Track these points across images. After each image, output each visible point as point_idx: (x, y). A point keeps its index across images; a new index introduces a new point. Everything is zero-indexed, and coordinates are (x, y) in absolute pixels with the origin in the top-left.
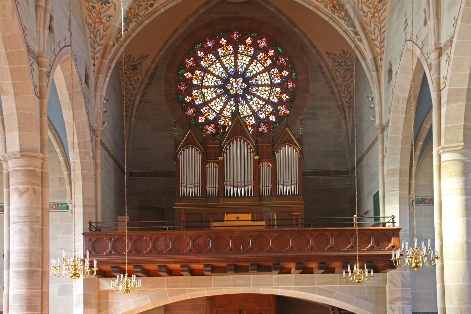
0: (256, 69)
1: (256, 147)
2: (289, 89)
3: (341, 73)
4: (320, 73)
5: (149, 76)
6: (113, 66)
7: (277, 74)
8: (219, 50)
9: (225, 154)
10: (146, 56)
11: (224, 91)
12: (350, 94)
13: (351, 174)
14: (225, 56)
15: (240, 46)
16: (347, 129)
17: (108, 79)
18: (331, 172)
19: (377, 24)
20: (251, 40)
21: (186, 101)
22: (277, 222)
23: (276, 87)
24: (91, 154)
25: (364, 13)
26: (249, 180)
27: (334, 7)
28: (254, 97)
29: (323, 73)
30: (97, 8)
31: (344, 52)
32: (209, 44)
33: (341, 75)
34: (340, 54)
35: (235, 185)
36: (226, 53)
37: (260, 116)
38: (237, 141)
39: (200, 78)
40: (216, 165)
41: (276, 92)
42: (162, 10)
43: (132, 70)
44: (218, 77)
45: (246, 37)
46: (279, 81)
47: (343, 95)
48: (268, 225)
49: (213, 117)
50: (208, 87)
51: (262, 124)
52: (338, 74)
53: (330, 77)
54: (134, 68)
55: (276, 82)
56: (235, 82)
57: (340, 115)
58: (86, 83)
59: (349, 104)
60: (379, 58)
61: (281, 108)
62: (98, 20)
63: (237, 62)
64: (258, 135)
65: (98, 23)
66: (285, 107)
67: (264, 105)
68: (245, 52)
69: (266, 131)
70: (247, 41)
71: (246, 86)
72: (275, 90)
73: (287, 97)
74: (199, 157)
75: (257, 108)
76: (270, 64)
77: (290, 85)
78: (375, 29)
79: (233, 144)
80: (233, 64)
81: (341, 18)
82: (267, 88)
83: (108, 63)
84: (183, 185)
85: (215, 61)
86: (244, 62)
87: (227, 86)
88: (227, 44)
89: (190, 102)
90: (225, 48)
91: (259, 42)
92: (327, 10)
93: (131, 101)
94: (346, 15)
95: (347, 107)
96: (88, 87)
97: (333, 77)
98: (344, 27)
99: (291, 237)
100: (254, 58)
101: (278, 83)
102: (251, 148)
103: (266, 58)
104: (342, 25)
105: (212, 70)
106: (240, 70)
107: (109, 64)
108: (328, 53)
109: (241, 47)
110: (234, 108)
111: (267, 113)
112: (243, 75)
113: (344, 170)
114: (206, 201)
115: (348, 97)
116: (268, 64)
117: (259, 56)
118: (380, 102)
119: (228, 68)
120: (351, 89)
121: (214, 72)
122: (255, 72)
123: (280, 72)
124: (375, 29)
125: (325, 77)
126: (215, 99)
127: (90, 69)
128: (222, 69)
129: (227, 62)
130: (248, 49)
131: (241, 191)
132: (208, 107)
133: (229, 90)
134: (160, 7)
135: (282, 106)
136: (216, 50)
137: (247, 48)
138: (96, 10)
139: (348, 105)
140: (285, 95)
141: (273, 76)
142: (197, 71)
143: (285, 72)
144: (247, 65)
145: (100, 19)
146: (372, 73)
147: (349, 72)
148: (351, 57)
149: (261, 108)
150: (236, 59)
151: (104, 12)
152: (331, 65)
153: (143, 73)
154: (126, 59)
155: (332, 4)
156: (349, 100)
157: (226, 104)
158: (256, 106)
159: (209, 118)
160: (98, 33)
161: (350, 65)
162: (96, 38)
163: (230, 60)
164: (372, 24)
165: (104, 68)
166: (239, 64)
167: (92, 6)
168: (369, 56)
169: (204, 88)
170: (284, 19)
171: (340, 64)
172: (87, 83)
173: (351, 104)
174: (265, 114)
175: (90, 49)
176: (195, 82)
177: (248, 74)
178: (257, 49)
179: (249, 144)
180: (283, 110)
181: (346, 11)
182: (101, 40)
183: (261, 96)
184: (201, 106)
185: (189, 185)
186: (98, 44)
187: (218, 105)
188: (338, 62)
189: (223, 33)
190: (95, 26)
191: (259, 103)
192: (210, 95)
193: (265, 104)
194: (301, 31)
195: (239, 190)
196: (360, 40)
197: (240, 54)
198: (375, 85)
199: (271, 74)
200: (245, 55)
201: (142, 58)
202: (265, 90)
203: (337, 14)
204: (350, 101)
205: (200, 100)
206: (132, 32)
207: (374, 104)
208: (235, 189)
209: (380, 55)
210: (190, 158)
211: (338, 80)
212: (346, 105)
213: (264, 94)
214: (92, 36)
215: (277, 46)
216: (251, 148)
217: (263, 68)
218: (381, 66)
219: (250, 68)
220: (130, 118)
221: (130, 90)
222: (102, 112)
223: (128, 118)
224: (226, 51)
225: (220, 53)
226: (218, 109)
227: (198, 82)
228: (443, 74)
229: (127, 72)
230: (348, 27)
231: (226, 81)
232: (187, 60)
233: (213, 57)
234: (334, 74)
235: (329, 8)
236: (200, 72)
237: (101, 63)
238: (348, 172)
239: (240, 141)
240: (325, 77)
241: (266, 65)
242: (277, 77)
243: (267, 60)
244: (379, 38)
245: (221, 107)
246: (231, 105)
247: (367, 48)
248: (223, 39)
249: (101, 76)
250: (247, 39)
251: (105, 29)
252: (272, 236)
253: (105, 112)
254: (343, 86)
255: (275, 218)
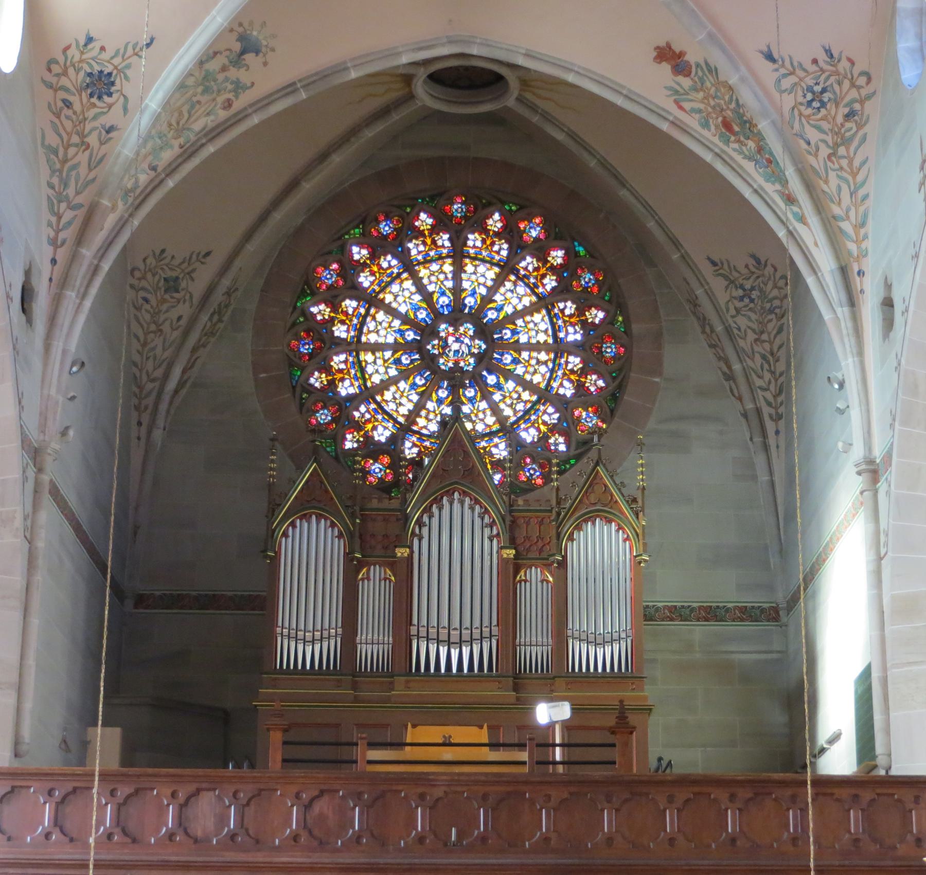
0: (515, 301)
1: (508, 519)
2: (606, 362)
3: (750, 319)
4: (693, 318)
5: (212, 310)
6: (106, 266)
7: (571, 316)
8: (410, 245)
9: (416, 541)
10: (208, 254)
11: (422, 358)
12: (776, 380)
13: (784, 619)
14: (427, 262)
15: (470, 236)
16: (772, 484)
17: (88, 303)
18: (727, 610)
19: (845, 174)
20: (501, 220)
21: (312, 386)
22: (563, 754)
23: (569, 354)
24: (18, 522)
25: (809, 143)
26: (486, 622)
27: (727, 125)
28: (506, 380)
29: (703, 321)
30: (77, 107)
31: (758, 261)
32: (385, 228)
33: (750, 324)
34: (747, 266)
35: (443, 637)
36: (432, 253)
37: (523, 435)
38: (451, 503)
39: (355, 321)
40: (389, 572)
41: (570, 367)
42: (255, 120)
43: (166, 291)
44: (405, 319)
45: (486, 212)
46: (578, 337)
47: (759, 382)
48: (538, 763)
49: (387, 433)
50: (375, 348)
51: (528, 460)
52: (742, 322)
53: (719, 328)
54: (172, 285)
55: (571, 338)
56: (453, 335)
57: (751, 439)
58: (24, 310)
59: (776, 408)
60: (856, 270)
61: (584, 414)
62: (75, 139)
63: (461, 280)
64: (515, 489)
65: (76, 145)
66: (595, 412)
67: (535, 404)
68: (484, 253)
69: (539, 481)
70: (490, 222)
71: (484, 347)
72: (567, 363)
73: (601, 383)
74: (338, 548)
75: (515, 412)
76: (553, 289)
77: (610, 350)
78: (839, 188)
79: (440, 509)
80: (449, 284)
81: (745, 157)
82: (543, 356)
83: (94, 257)
84: (285, 631)
85: (399, 275)
86: (482, 280)
87: (429, 347)
88: (434, 230)
89: (323, 389)
90: (429, 241)
91: (522, 226)
92: (711, 136)
93: (153, 380)
94: (760, 150)
95: (771, 416)
96: (29, 321)
97: (728, 330)
98: (755, 181)
99: (608, 802)
100: (507, 269)
101: (575, 344)
102: (491, 525)
103: (543, 271)
104: (749, 174)
105: (389, 298)
106: (470, 301)
107: (96, 262)
108: (714, 264)
109: (474, 240)
110: (448, 410)
111: (543, 428)
112: (476, 317)
113: (766, 605)
114: (355, 686)
115: (772, 387)
116: (548, 288)
117: (523, 264)
118: (862, 395)
119: (435, 296)
120: (781, 367)
121: (394, 305)
122: (509, 310)
123: (580, 311)
124: (839, 188)
125: (708, 329)
126: (394, 381)
127: (40, 272)
128: (417, 298)
129: (433, 279)
130: (493, 244)
131: (458, 657)
132: (373, 406)
133: (434, 358)
134: (250, 111)
135: (586, 410)
136: (401, 244)
137: (488, 242)
138: (75, 113)
139: (773, 411)
140: (594, 377)
141: (560, 322)
142: (348, 302)
143: (594, 311)
144: (489, 289)
145: (82, 136)
146: (839, 310)
147: (773, 316)
148: (778, 275)
149: (527, 412)
150: (459, 270)
151: (95, 118)
152: (722, 297)
153: (196, 301)
154: (151, 261)
155: (720, 119)
156: (775, 397)
157: (425, 396)
158: (511, 406)
159: (376, 438)
160: (74, 173)
161: (775, 298)
162: (66, 185)
163: (442, 272)
164: (832, 175)
165: (81, 272)
166: (466, 285)
167: (64, 101)
168: (826, 261)
169: (366, 350)
170: (593, 163)
171: (747, 294)
172: (25, 308)
173: (781, 410)
174: (538, 429)
175: (47, 216)
176: (340, 331)
177: (492, 315)
178: (518, 247)
179: (487, 512)
180: (588, 419)
181: (759, 138)
182: (78, 193)
183: (528, 377)
184: (353, 400)
185: (304, 633)
186: (69, 202)
187: (404, 401)
188: (742, 287)
189: (423, 200)
190: (66, 154)
191: (519, 397)
192: (382, 370)
193: (538, 402)
194: (636, 198)
195: (455, 654)
196: (802, 219)
197: (469, 257)
198: (847, 346)
199: (556, 315)
200: (483, 261)
201: (194, 256)
202: (539, 362)
203: (736, 146)
204: (779, 399)
205: (352, 385)
206: (167, 175)
207: (846, 400)
208: (443, 651)
209: (858, 259)
210: (311, 552)
211: (744, 339)
212: (766, 411)
213: (535, 372)
214: (55, 181)
215: (574, 240)
216: (491, 525)
217: (534, 299)
218: (862, 291)
219: (498, 297)
220: (149, 432)
221: (154, 349)
222: (61, 399)
223: (144, 429)
224: (430, 250)
225: (414, 252)
226: (404, 410)
227: (348, 331)
228: (883, 525)
229: (149, 296)
230: (767, 181)
231: (428, 331)
232: (320, 269)
233: (394, 262)
234: (730, 321)
235: (713, 128)
236: (354, 304)
237: (74, 257)
238: (777, 612)
239: (462, 503)
240: (708, 329)
241: (541, 290)
242: (573, 325)
243: (544, 276)
244: (852, 214)
245: (411, 406)
246: (440, 402)
247: (822, 239)
248: (423, 216)
249: (71, 295)
250: (490, 216)
251: (93, 165)
252: (549, 797)
253: (73, 398)
254: (757, 355)
255: (558, 741)
